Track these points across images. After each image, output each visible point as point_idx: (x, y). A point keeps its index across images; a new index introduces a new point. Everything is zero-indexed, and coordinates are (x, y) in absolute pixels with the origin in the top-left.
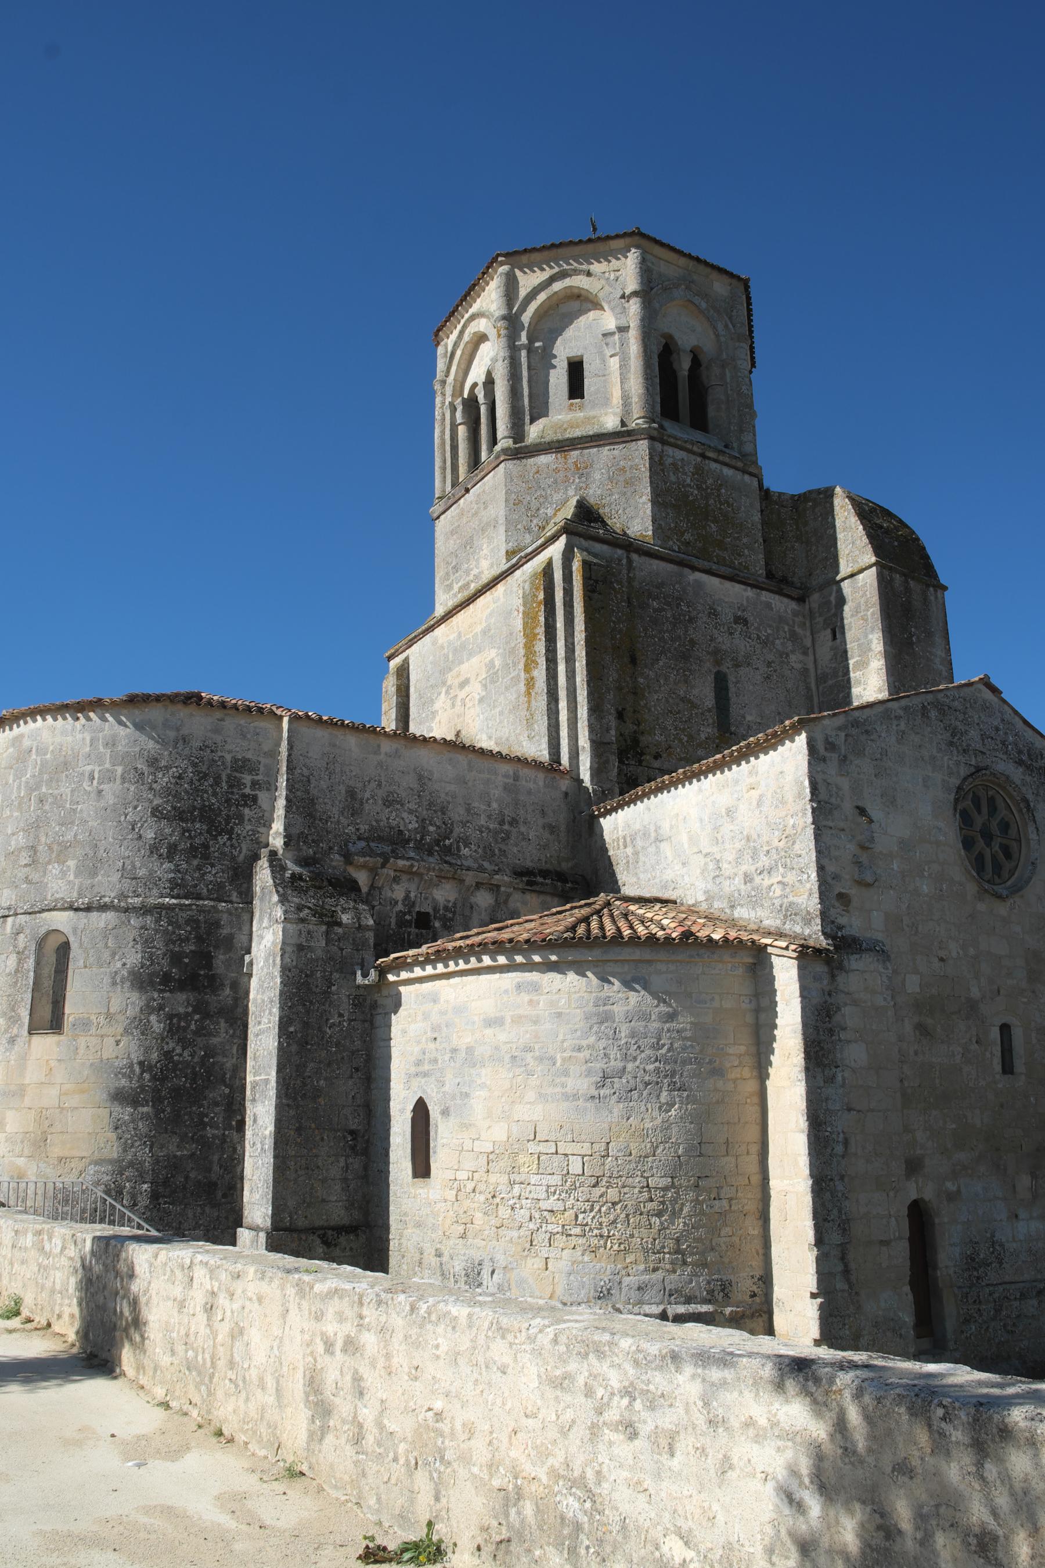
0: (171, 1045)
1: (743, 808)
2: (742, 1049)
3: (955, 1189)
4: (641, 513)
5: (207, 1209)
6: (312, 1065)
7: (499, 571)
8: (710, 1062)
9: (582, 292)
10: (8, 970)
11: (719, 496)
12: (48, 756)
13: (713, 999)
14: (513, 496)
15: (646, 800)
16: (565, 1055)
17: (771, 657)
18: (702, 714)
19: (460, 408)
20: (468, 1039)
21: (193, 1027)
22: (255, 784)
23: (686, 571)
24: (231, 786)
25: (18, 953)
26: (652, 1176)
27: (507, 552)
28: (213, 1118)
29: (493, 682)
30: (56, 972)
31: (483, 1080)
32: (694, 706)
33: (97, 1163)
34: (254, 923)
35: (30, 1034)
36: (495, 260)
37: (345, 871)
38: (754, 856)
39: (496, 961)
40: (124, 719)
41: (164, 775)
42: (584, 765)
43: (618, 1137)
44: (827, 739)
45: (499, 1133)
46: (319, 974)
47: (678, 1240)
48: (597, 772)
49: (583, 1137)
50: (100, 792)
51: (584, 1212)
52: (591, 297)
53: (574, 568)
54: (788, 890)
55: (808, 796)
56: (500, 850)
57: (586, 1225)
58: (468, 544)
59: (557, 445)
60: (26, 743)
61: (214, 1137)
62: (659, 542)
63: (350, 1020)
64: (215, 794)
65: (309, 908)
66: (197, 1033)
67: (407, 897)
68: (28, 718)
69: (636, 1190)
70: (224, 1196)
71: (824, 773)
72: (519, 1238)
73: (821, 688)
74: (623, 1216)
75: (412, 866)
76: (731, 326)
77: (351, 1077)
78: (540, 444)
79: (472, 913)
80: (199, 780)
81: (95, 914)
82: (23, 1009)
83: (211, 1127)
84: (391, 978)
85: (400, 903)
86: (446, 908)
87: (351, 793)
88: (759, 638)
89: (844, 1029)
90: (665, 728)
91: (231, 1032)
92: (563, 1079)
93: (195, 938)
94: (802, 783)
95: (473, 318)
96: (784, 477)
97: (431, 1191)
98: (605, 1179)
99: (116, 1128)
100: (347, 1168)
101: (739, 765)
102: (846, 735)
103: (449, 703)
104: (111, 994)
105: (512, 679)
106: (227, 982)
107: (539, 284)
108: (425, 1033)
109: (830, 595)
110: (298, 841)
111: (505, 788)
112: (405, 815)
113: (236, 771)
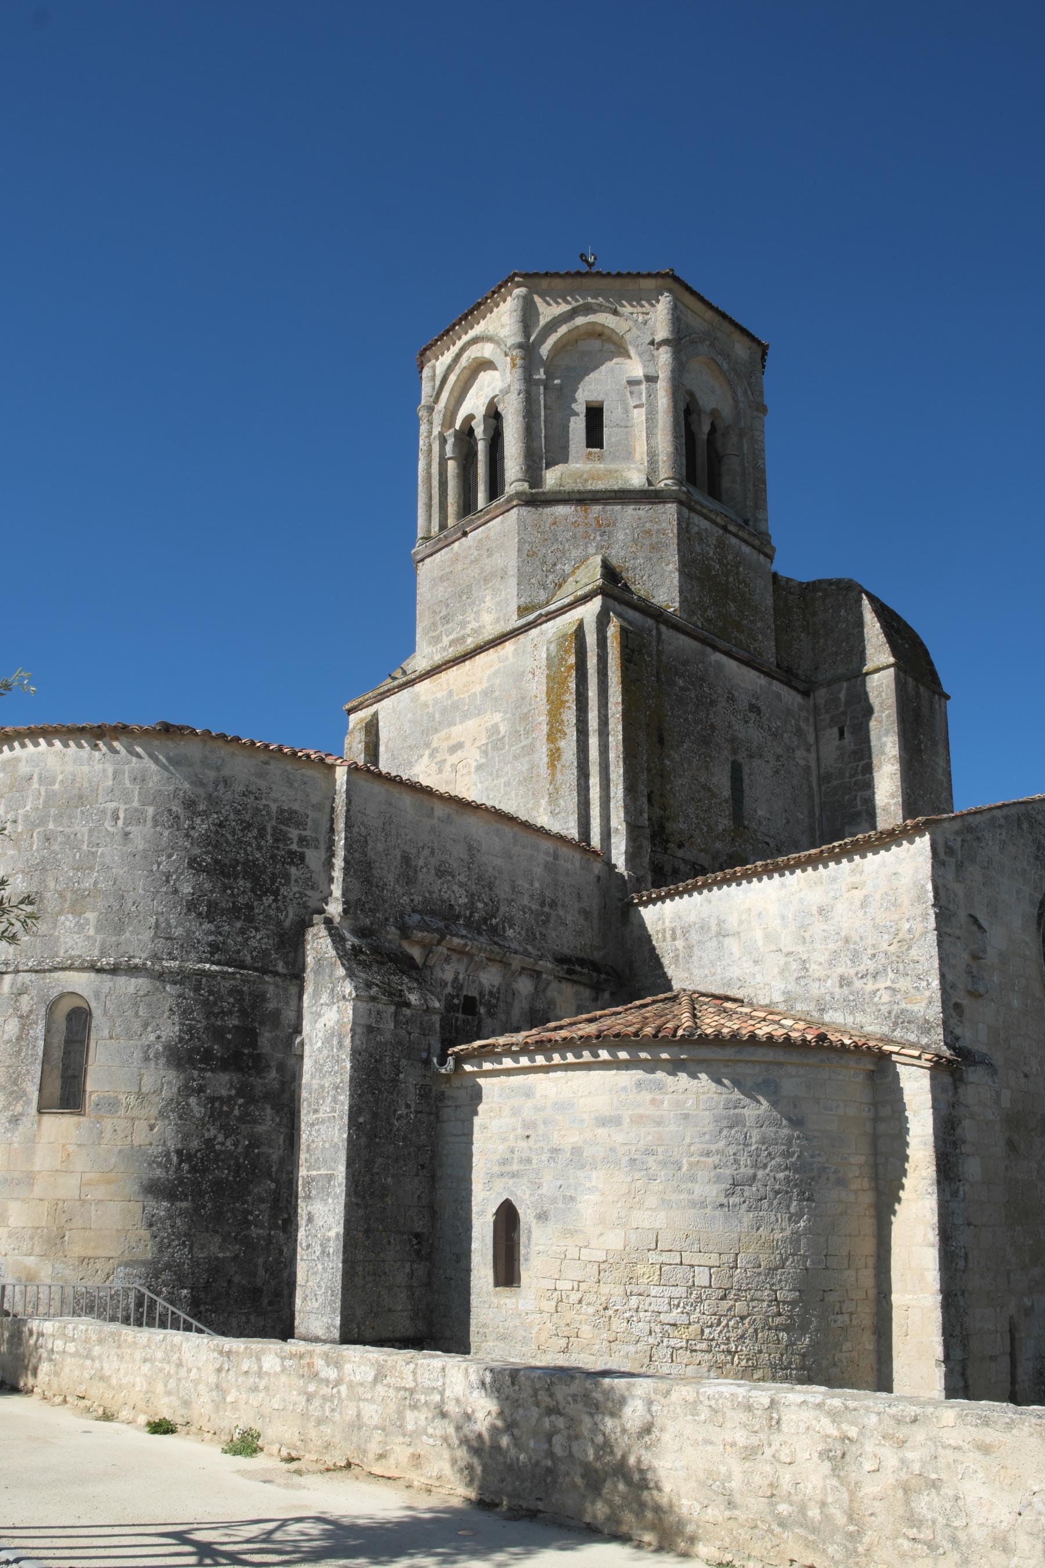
0: (213, 1132)
1: (840, 908)
2: (863, 1159)
3: (1029, 1304)
4: (668, 582)
5: (253, 1318)
6: (380, 1160)
7: (509, 627)
8: (836, 1172)
9: (607, 332)
10: (6, 1037)
11: (737, 573)
12: (57, 786)
13: (838, 1106)
14: (527, 546)
15: (705, 891)
16: (691, 1159)
17: (780, 751)
18: (720, 804)
19: (451, 441)
20: (573, 1139)
21: (236, 1112)
22: (302, 840)
23: (709, 650)
24: (276, 840)
25: (21, 1017)
26: (781, 1289)
27: (519, 607)
28: (258, 1216)
29: (496, 748)
30: (66, 1041)
31: (594, 1183)
32: (713, 795)
33: (127, 1265)
34: (305, 997)
35: (40, 1112)
36: (511, 279)
37: (400, 946)
38: (855, 956)
39: (598, 1056)
40: (139, 749)
41: (203, 821)
42: (617, 848)
43: (748, 1248)
44: (946, 843)
45: (614, 1241)
46: (387, 1060)
47: (804, 1356)
48: (632, 857)
49: (711, 1248)
50: (127, 834)
51: (711, 1326)
52: (615, 337)
53: (609, 634)
54: (899, 996)
55: (931, 901)
56: (541, 933)
57: (713, 1340)
58: (465, 595)
59: (577, 496)
60: (24, 769)
61: (259, 1237)
62: (685, 617)
63: (417, 1112)
64: (259, 848)
65: (377, 985)
66: (241, 1119)
67: (456, 979)
68: (27, 741)
69: (765, 1304)
70: (270, 1303)
71: (944, 878)
72: (636, 1353)
73: (823, 788)
74: (751, 1330)
75: (466, 945)
76: (750, 393)
77: (417, 1175)
78: (560, 492)
79: (514, 1000)
80: (242, 831)
81: (122, 980)
82: (30, 1084)
83: (256, 1226)
84: (468, 1068)
85: (449, 985)
86: (491, 993)
87: (406, 859)
88: (770, 729)
89: (964, 1142)
90: (688, 816)
91: (278, 1120)
92: (690, 1185)
93: (239, 1011)
94: (923, 886)
95: (475, 340)
96: (798, 560)
97: (521, 1301)
98: (733, 1292)
99: (151, 1225)
100: (412, 1274)
101: (838, 862)
102: (963, 841)
103: (434, 768)
104: (143, 1071)
105: (523, 747)
106: (273, 1064)
107: (560, 315)
108: (514, 1130)
109: (839, 692)
110: (356, 909)
111: (546, 867)
112: (456, 888)
113: (282, 823)
